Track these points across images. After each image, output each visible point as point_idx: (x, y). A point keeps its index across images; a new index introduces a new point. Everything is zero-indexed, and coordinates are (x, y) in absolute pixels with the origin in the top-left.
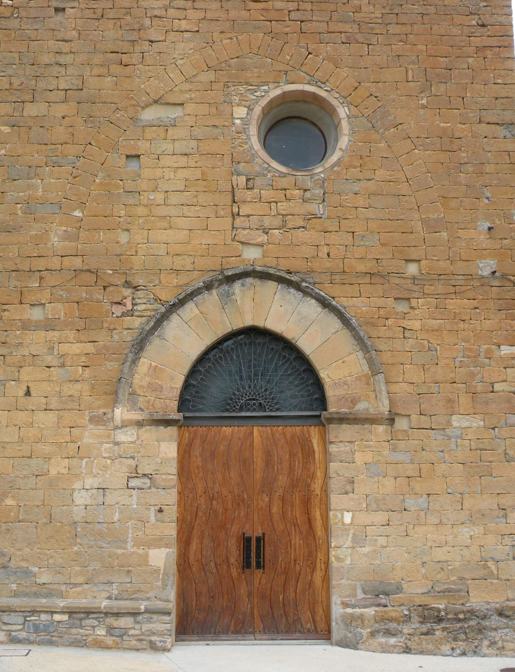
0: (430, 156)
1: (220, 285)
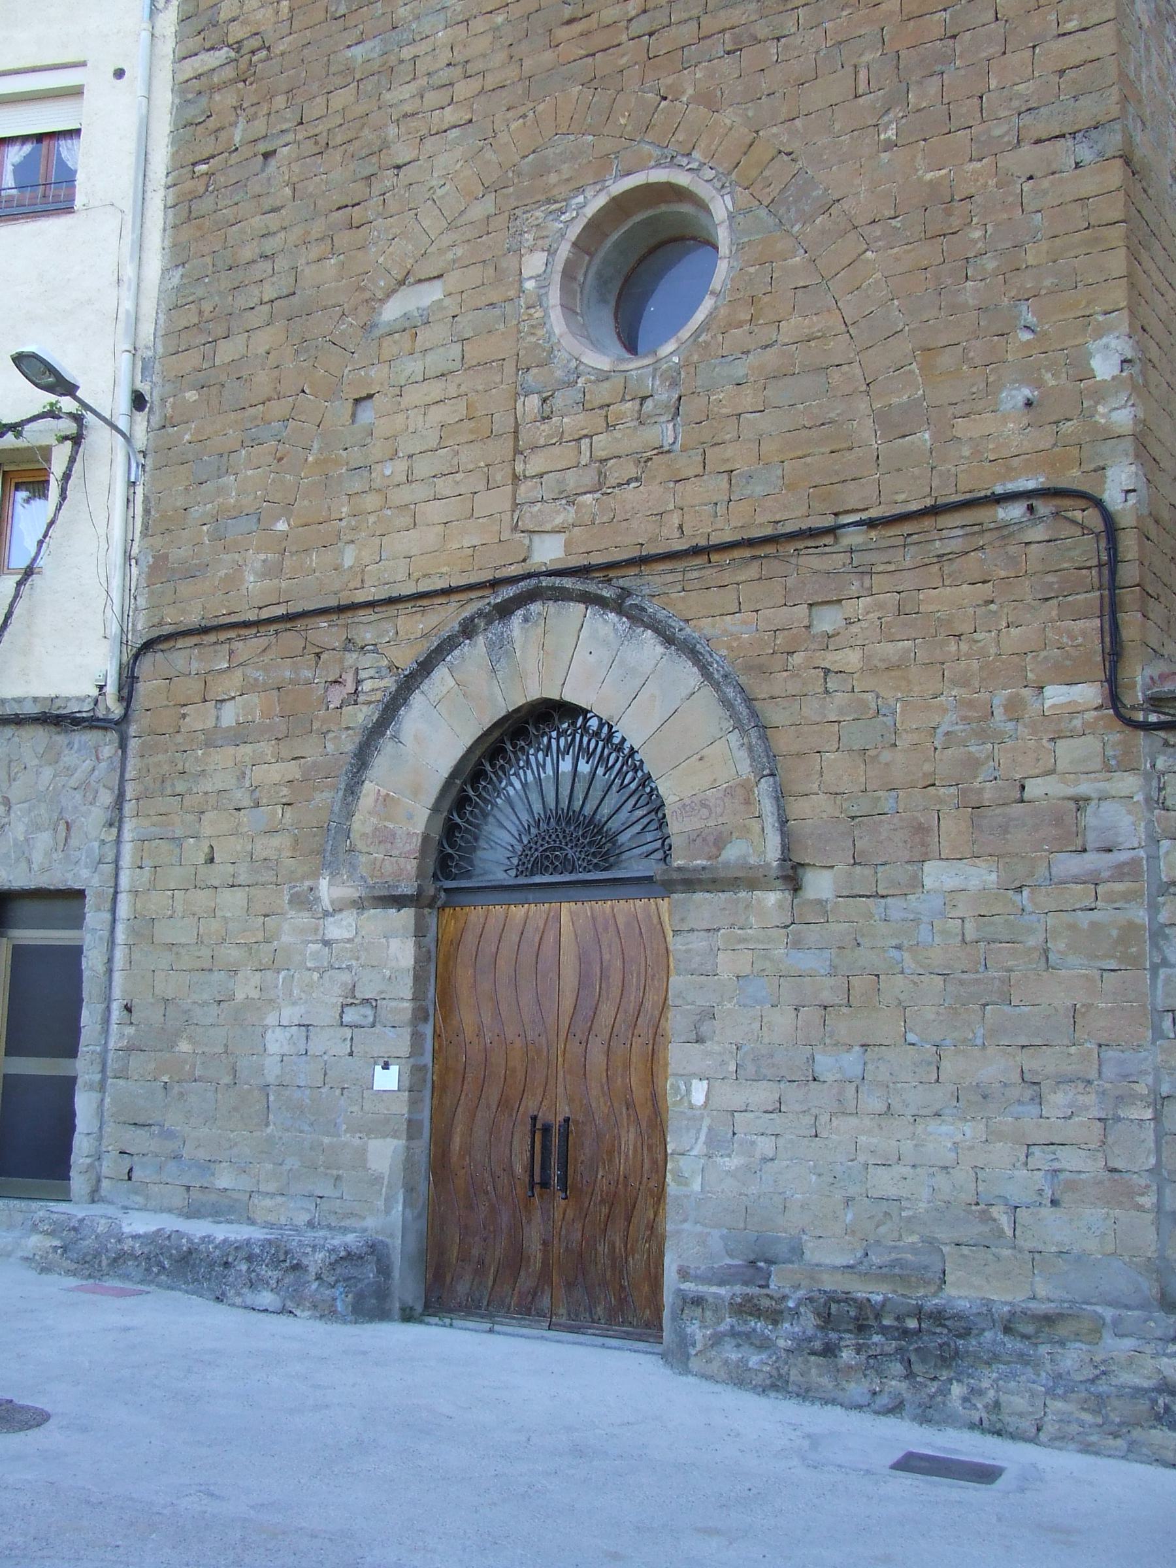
1: (490, 622)
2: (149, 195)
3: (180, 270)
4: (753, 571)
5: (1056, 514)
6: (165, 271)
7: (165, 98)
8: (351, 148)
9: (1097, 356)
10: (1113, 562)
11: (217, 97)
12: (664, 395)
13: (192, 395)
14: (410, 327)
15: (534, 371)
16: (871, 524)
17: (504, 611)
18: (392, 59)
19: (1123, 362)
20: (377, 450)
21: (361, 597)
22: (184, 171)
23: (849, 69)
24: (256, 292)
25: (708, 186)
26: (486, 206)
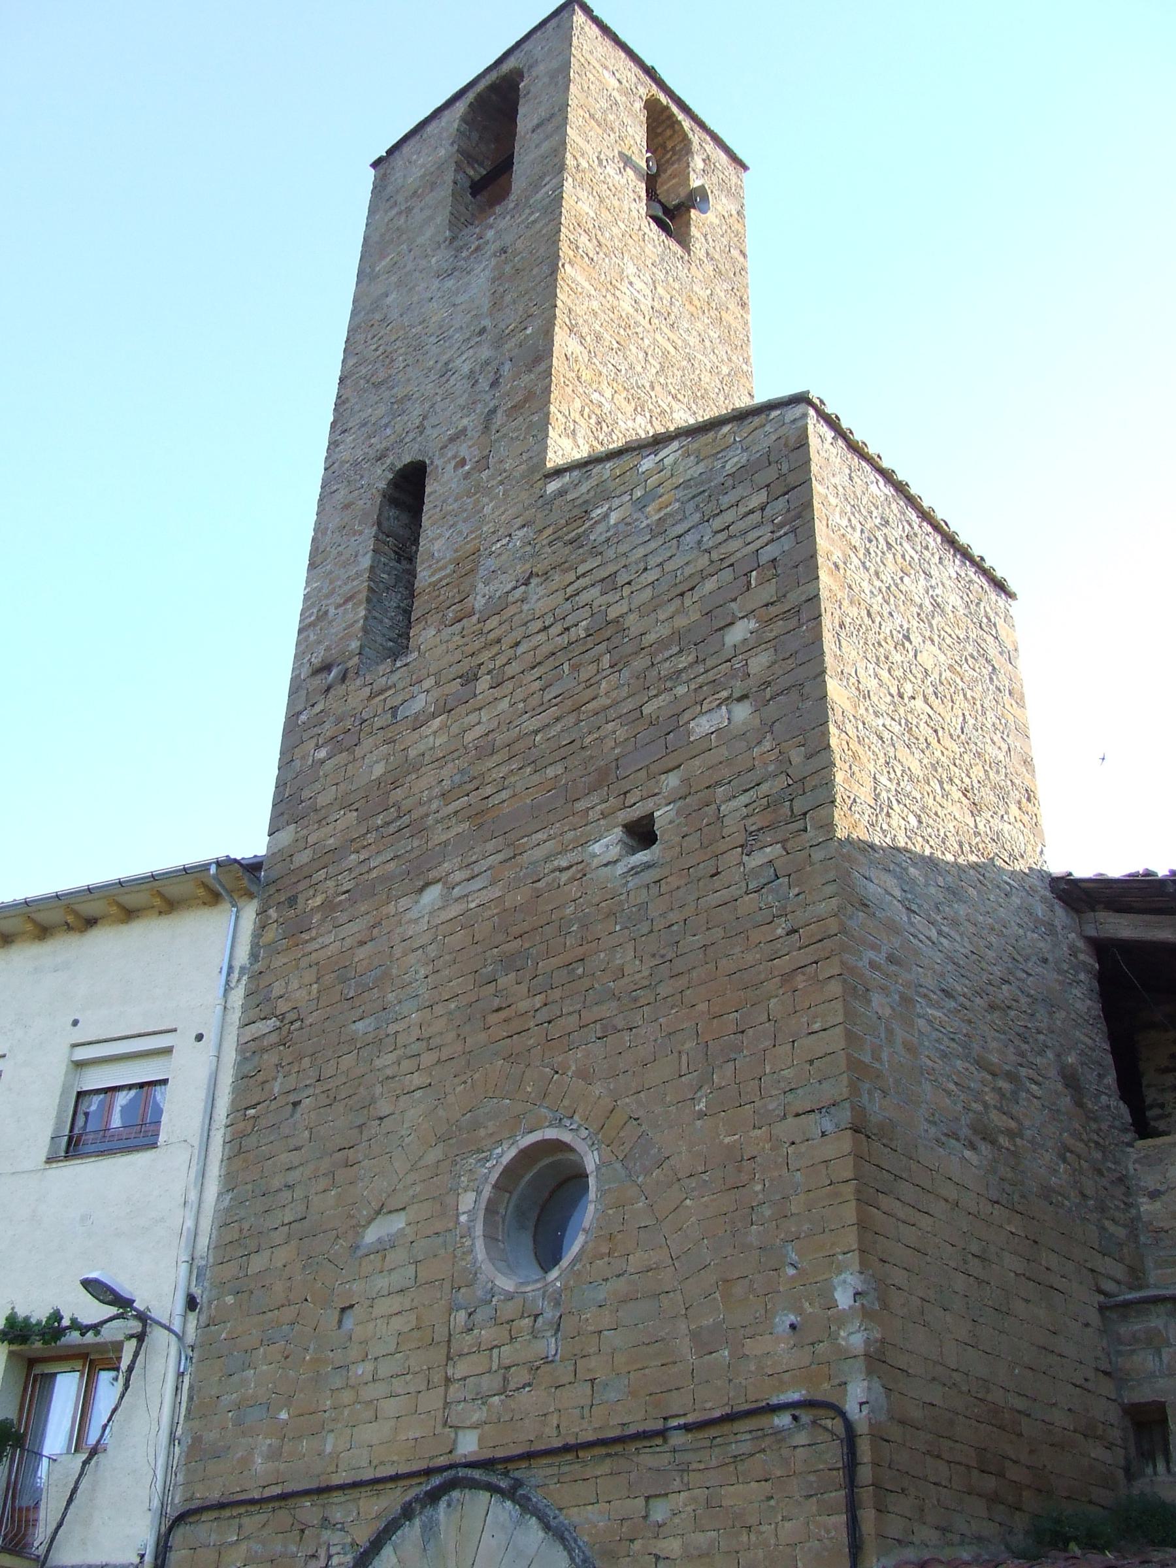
0: (707, 1206)
1: (423, 1507)
2: (212, 1133)
3: (230, 1195)
4: (605, 1468)
5: (814, 1422)
6: (220, 1195)
7: (230, 1056)
8: (351, 1102)
9: (839, 1289)
10: (851, 1464)
11: (265, 1056)
12: (550, 1314)
13: (230, 1300)
14: (382, 1249)
15: (463, 1290)
16: (687, 1428)
17: (433, 1497)
18: (382, 1035)
19: (855, 1294)
20: (354, 1352)
21: (336, 1480)
22: (239, 1114)
23: (676, 1054)
24: (280, 1216)
25: (583, 1143)
26: (433, 1156)
